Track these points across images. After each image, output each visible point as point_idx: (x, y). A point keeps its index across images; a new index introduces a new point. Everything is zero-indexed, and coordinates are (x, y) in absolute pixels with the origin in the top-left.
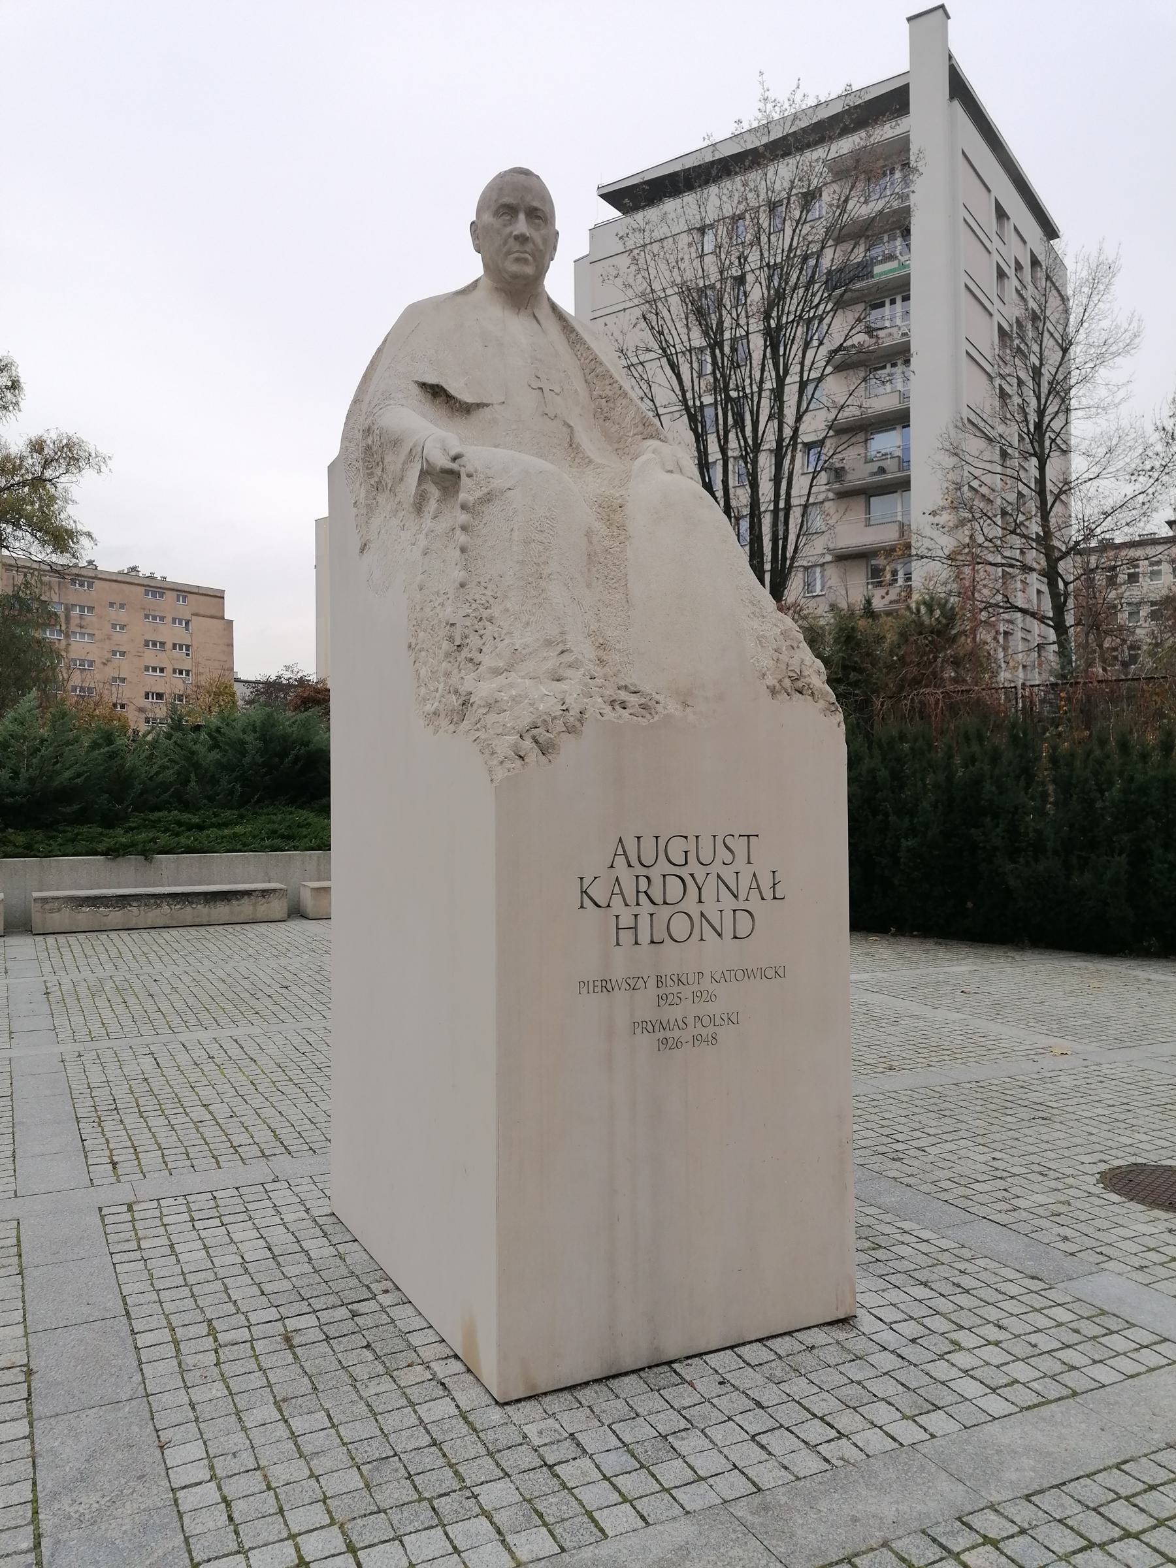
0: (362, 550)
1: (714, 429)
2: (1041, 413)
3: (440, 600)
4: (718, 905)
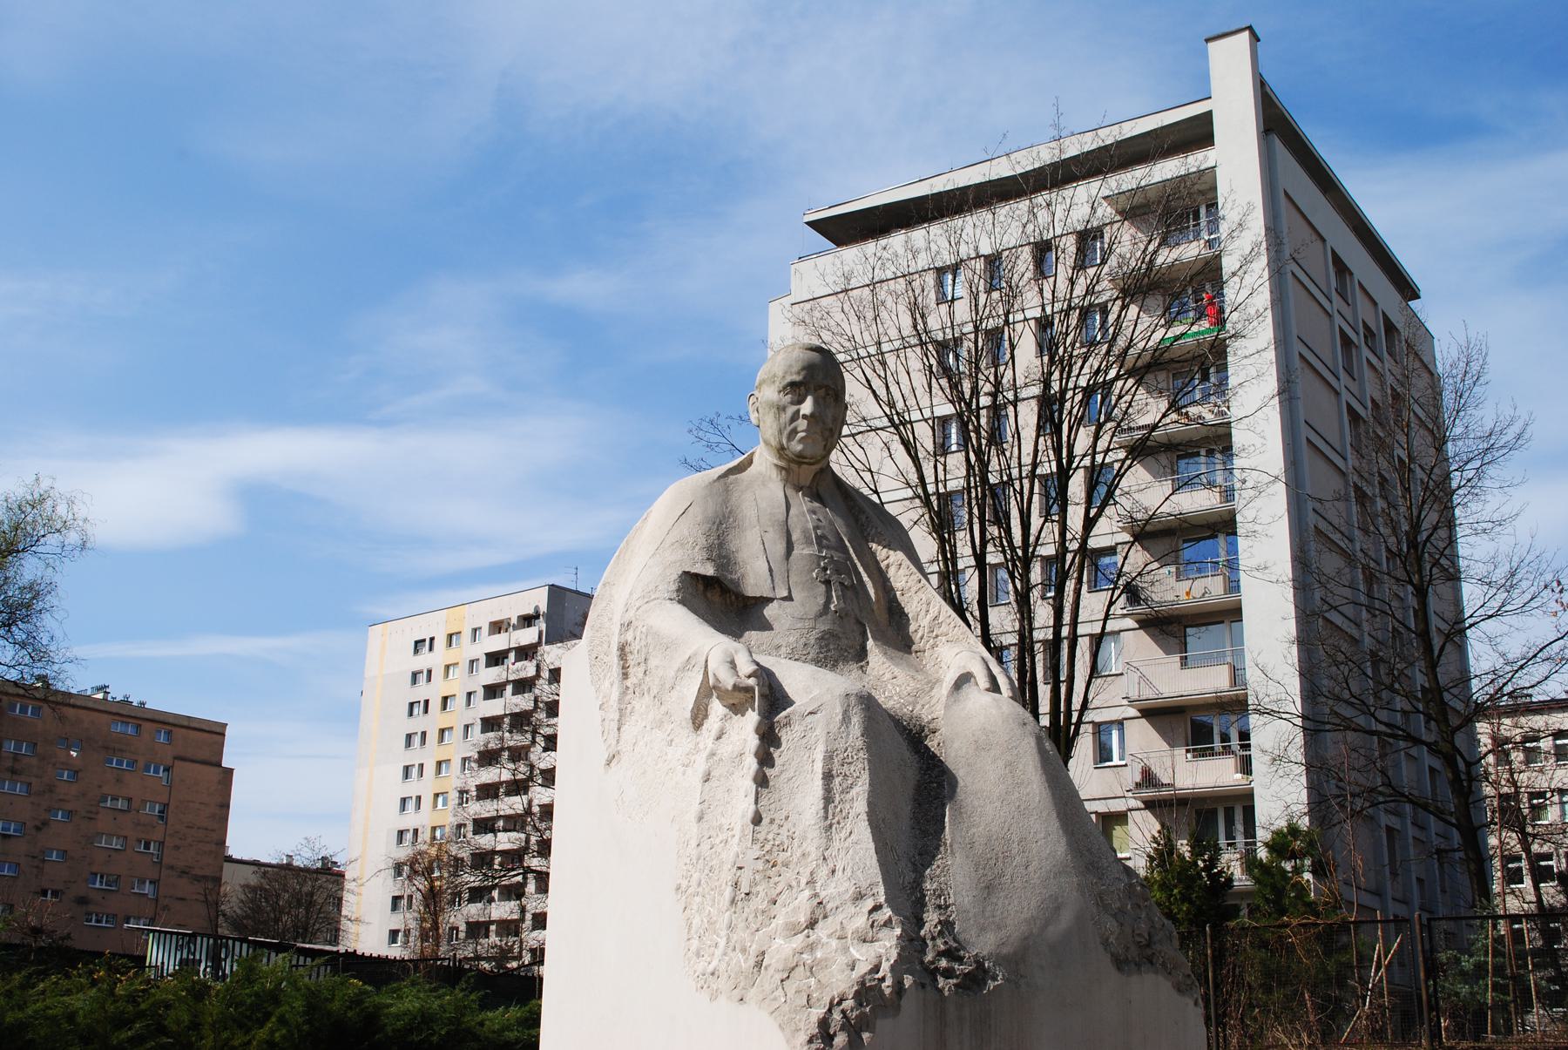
2: (1416, 526)
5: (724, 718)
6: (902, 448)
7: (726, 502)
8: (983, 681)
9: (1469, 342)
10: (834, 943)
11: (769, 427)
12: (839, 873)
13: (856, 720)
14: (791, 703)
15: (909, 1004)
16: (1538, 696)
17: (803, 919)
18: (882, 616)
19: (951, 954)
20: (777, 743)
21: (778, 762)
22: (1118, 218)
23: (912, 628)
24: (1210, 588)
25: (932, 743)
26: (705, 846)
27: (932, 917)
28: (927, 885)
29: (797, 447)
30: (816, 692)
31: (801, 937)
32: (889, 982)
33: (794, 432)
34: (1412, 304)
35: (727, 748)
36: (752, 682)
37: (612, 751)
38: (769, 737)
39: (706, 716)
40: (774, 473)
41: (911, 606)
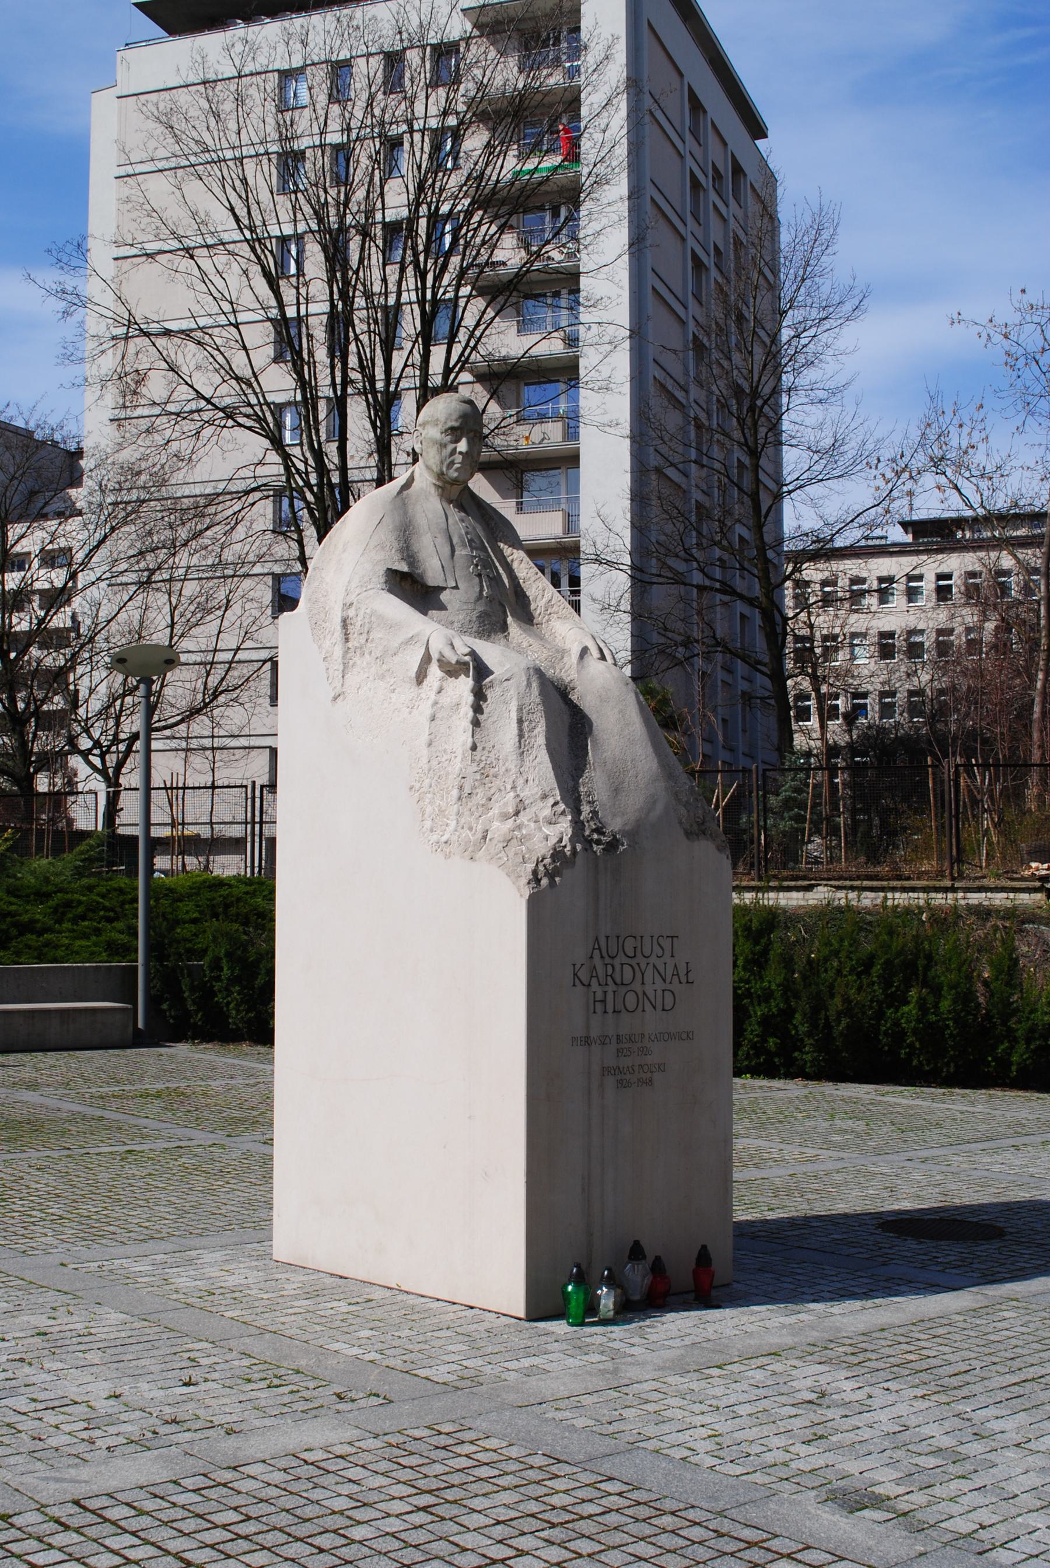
0: (335, 699)
1: (328, 381)
3: (445, 757)
4: (653, 987)
5: (442, 679)
6: (263, 281)
7: (405, 513)
8: (596, 654)
9: (821, 210)
10: (532, 825)
11: (431, 457)
12: (531, 782)
13: (535, 685)
14: (492, 673)
15: (579, 860)
16: (839, 543)
17: (511, 810)
18: (512, 598)
19: (599, 831)
20: (485, 699)
21: (486, 711)
22: (476, 33)
23: (532, 607)
24: (549, 435)
25: (574, 697)
26: (434, 763)
27: (586, 809)
28: (581, 789)
29: (453, 474)
30: (508, 666)
31: (511, 821)
32: (568, 848)
33: (452, 463)
34: (759, 143)
35: (445, 700)
36: (467, 658)
37: (338, 691)
38: (479, 695)
39: (425, 676)
40: (433, 490)
41: (531, 591)
